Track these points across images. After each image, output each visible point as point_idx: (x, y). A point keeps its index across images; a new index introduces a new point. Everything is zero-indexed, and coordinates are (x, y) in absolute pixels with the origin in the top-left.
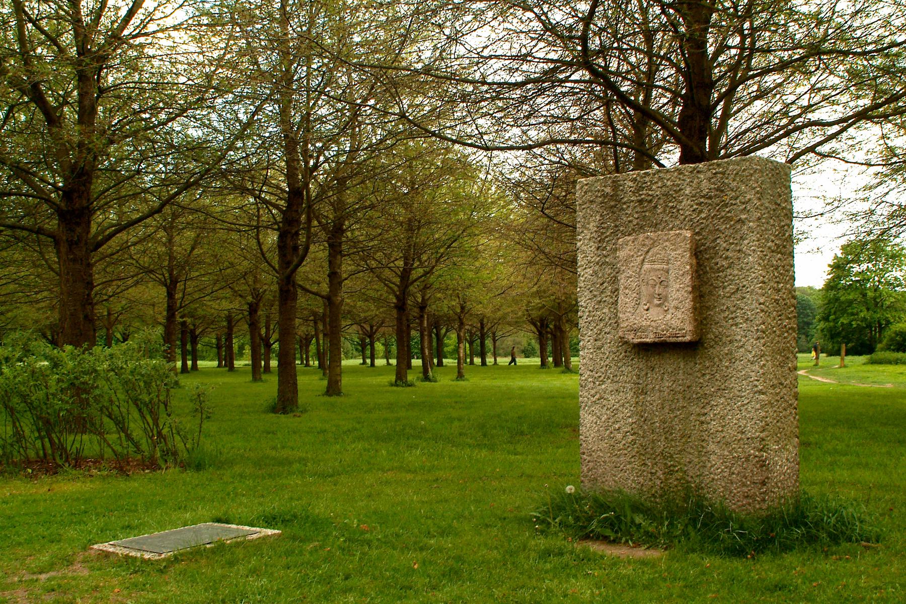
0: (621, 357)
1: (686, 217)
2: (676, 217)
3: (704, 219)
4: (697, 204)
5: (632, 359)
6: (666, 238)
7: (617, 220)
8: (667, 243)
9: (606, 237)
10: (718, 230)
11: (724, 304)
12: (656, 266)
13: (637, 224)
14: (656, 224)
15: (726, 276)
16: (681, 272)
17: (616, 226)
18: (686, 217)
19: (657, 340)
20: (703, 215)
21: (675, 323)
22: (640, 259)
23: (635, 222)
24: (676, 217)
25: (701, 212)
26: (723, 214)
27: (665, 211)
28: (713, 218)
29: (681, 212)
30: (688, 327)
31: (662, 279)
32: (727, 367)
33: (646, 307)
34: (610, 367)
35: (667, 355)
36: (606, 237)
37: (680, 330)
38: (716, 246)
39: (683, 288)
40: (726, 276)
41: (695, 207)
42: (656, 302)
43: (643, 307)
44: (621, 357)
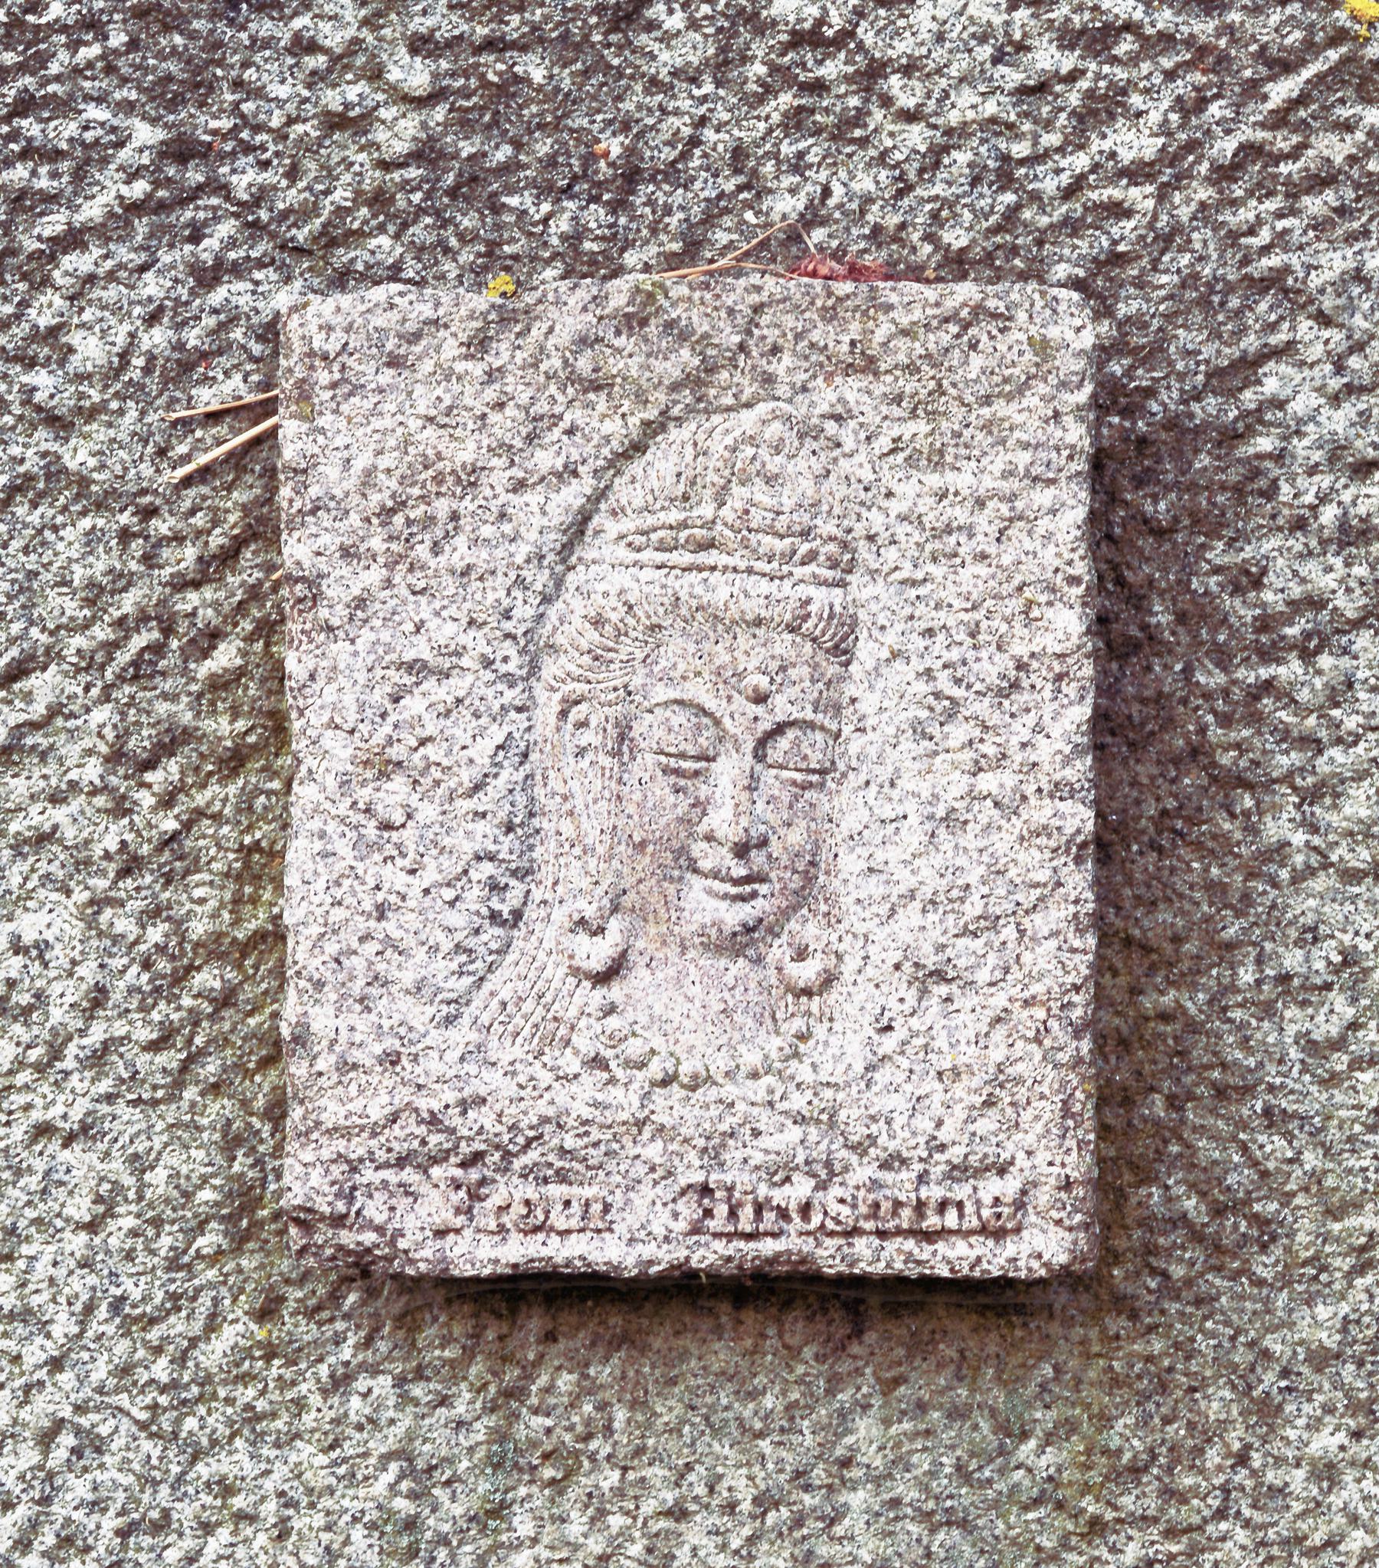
0: (214, 1353)
1: (956, 135)
2: (846, 130)
3: (1137, 173)
4: (1068, 37)
5: (340, 1383)
6: (839, 339)
7: (199, 86)
8: (852, 389)
9: (73, 239)
10: (1274, 281)
11: (1311, 936)
12: (720, 591)
13: (427, 153)
14: (631, 175)
15: (1341, 692)
16: (991, 668)
17: (181, 150)
18: (956, 135)
19: (707, 1255)
20: (1132, 142)
21: (916, 1110)
22: (543, 513)
23: (400, 131)
24: (846, 130)
25: (1104, 108)
26: (1334, 148)
27: (724, 65)
28: (1224, 174)
29: (904, 92)
30: (1046, 1153)
31: (782, 707)
32: (1327, 1473)
33: (597, 953)
34: (92, 1444)
35: (722, 1354)
36: (73, 239)
37: (959, 1172)
38: (1254, 420)
39: (1008, 807)
40: (1341, 692)
41: (1047, 57)
42: (706, 906)
43: (550, 947)
44: (214, 1353)
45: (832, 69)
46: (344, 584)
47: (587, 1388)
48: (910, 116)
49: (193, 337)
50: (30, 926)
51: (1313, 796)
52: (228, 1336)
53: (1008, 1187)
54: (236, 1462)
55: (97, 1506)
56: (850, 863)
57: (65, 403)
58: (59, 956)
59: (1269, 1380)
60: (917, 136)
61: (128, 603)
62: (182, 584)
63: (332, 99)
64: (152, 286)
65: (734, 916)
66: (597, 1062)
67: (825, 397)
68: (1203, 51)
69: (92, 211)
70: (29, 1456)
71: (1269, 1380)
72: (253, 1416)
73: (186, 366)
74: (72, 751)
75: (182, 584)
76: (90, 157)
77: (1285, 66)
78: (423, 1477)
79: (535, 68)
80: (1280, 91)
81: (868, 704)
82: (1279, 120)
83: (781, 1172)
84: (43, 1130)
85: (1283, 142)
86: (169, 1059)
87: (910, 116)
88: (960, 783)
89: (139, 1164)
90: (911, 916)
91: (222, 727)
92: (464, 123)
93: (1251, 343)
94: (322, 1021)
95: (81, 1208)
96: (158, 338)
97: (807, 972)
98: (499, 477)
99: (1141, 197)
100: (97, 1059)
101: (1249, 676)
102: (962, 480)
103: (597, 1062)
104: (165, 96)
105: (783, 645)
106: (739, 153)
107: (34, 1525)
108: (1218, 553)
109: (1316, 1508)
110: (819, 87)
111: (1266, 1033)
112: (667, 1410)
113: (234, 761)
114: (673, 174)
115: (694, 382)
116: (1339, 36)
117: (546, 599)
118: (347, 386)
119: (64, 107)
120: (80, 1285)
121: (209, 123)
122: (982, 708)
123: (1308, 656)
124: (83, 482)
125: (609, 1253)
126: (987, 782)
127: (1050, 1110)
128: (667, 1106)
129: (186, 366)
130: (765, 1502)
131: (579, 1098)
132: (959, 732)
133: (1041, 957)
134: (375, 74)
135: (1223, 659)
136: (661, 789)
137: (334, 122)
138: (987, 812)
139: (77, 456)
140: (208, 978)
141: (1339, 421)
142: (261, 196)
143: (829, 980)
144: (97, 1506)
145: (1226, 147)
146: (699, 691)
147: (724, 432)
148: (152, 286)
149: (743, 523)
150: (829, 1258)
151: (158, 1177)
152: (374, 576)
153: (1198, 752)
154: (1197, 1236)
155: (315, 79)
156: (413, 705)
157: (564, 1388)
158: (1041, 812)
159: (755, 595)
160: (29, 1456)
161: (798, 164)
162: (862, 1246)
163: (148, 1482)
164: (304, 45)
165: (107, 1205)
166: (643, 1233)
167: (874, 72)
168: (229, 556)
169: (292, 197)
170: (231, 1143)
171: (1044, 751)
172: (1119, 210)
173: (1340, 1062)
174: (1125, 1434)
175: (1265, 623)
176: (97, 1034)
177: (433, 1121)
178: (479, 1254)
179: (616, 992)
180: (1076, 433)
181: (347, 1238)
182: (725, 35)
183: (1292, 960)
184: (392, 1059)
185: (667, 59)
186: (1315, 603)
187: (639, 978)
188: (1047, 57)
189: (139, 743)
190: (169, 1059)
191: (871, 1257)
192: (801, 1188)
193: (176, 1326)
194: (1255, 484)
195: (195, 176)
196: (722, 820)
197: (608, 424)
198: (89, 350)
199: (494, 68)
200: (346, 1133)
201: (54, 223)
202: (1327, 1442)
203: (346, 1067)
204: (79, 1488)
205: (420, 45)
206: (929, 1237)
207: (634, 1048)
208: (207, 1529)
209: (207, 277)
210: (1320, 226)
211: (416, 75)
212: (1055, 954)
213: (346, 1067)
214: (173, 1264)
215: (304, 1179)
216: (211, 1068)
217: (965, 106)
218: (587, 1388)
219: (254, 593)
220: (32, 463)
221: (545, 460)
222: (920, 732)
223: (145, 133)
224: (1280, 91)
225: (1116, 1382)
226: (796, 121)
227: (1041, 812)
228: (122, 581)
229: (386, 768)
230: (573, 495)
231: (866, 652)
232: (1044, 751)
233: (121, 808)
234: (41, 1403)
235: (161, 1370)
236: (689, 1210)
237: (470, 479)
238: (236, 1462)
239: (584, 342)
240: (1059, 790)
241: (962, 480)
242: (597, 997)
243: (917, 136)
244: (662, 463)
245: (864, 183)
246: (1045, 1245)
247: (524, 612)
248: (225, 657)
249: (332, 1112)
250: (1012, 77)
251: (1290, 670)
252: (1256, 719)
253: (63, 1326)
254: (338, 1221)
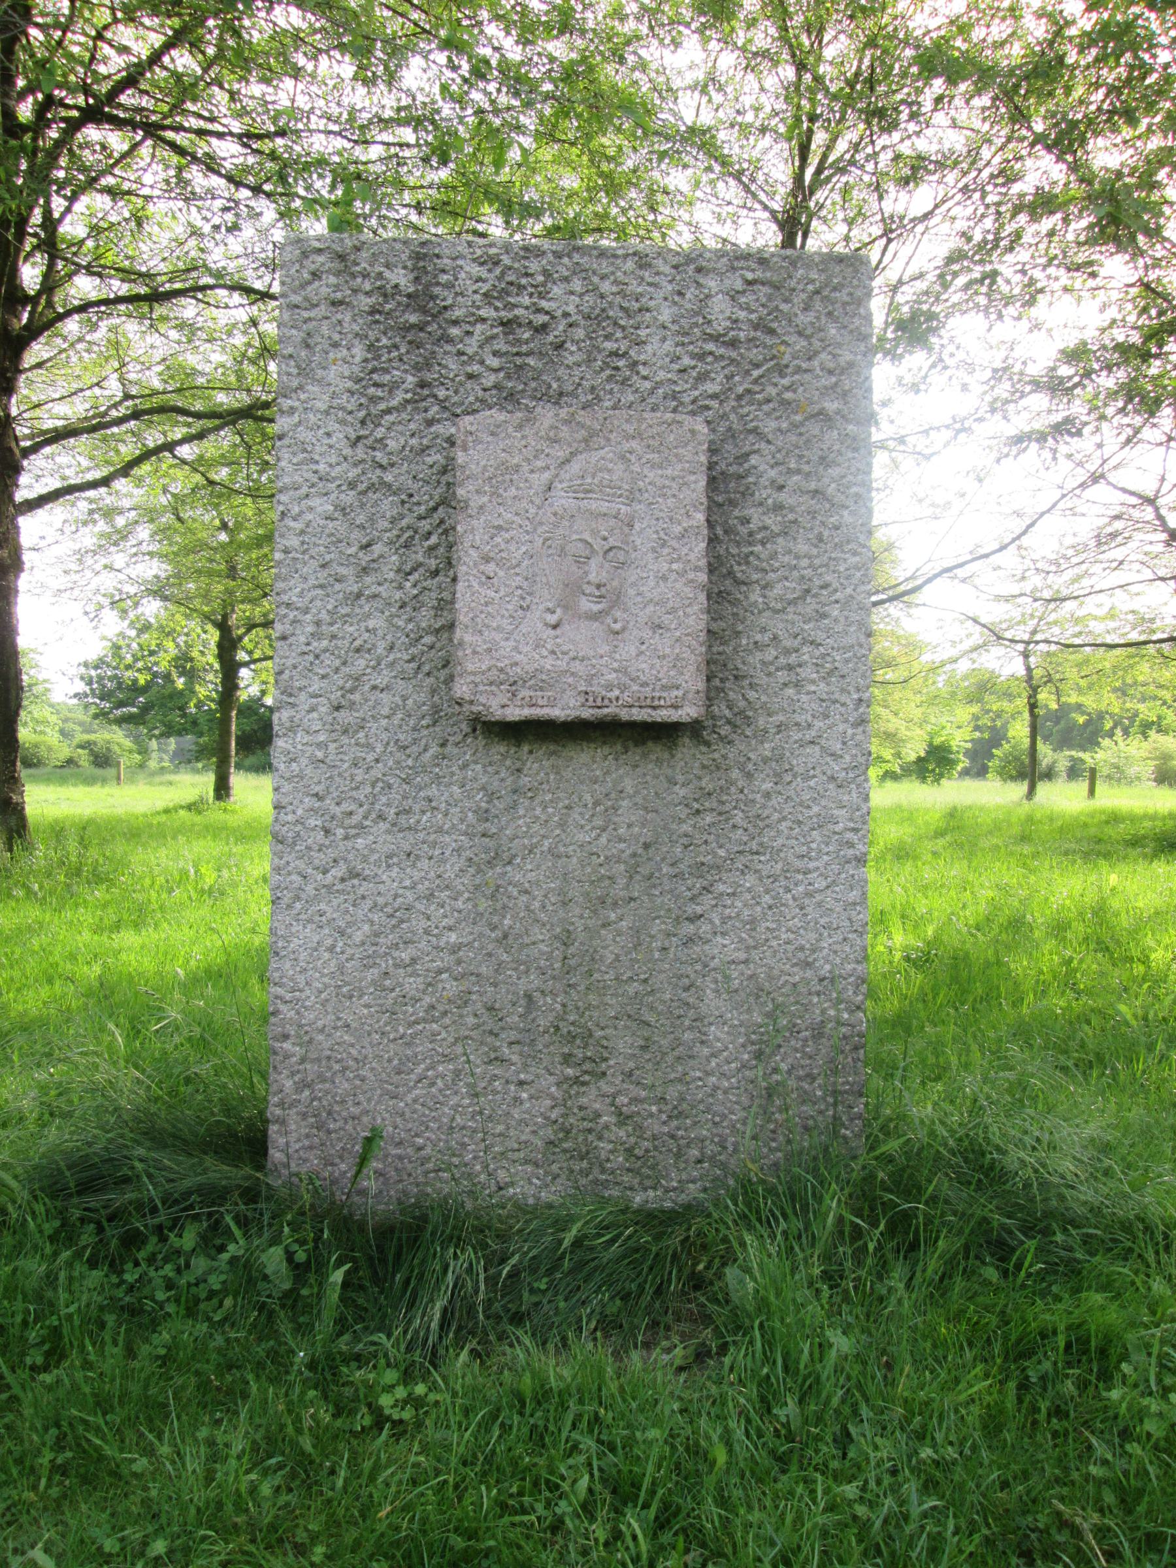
1: (658, 385)
3: (714, 396)
4: (693, 356)
5: (465, 766)
7: (428, 366)
8: (634, 444)
9: (388, 411)
10: (754, 431)
11: (764, 630)
12: (594, 505)
13: (497, 386)
16: (677, 529)
17: (422, 384)
18: (658, 385)
20: (711, 388)
23: (490, 380)
25: (703, 377)
27: (590, 361)
28: (739, 398)
29: (644, 371)
30: (692, 681)
31: (612, 542)
32: (767, 795)
33: (552, 619)
36: (388, 411)
37: (664, 688)
38: (748, 473)
41: (687, 361)
45: (621, 363)
46: (476, 501)
47: (542, 768)
48: (645, 378)
49: (425, 442)
50: (371, 624)
51: (764, 587)
52: (431, 752)
53: (680, 693)
54: (433, 791)
55: (388, 805)
56: (632, 592)
57: (384, 462)
58: (380, 633)
59: (750, 766)
60: (647, 385)
61: (404, 523)
62: (420, 518)
63: (469, 369)
64: (412, 426)
65: (596, 608)
66: (553, 652)
67: (627, 446)
68: (733, 360)
69: (394, 403)
70: (368, 789)
71: (750, 766)
72: (438, 777)
73: (424, 450)
74: (385, 569)
75: (420, 518)
76: (393, 387)
77: (757, 366)
78: (491, 796)
79: (531, 361)
80: (756, 373)
81: (638, 542)
82: (756, 382)
83: (609, 687)
84: (374, 688)
85: (757, 388)
86: (413, 665)
87: (645, 378)
88: (666, 566)
89: (405, 699)
90: (651, 608)
91: (433, 563)
92: (508, 377)
93: (747, 449)
94: (468, 638)
95: (386, 711)
96: (414, 442)
97: (617, 626)
98: (526, 468)
99: (714, 404)
100: (392, 664)
101: (745, 550)
102: (669, 472)
103: (553, 652)
104: (417, 368)
105: (612, 522)
106: (593, 388)
107: (369, 812)
108: (736, 513)
109: (764, 807)
110: (617, 369)
111: (750, 659)
112: (567, 773)
113: (435, 573)
114: (573, 394)
115: (586, 441)
116: (773, 357)
117: (615, 324)
118: (477, 441)
119: (386, 371)
120: (385, 736)
121: (429, 376)
122: (674, 543)
123: (763, 544)
124: (390, 486)
125: (558, 713)
126: (675, 566)
127: (692, 668)
128: (577, 666)
129: (424, 450)
130: (597, 803)
131: (548, 663)
132: (666, 551)
133: (691, 621)
134: (482, 362)
135: (738, 544)
136: (574, 568)
137: (470, 376)
138: (674, 576)
139: (389, 478)
140: (428, 640)
141: (773, 473)
142: (447, 398)
143: (624, 629)
144: (388, 805)
145: (740, 390)
146: (587, 536)
147: (595, 456)
148: (412, 426)
149: (601, 484)
150: (625, 715)
151: (410, 702)
152: (485, 499)
153: (730, 573)
154: (729, 722)
155: (464, 363)
156: (498, 540)
157: (537, 764)
158: (691, 575)
159: (604, 507)
160: (368, 789)
161: (611, 392)
162: (634, 711)
163: (405, 798)
164: (460, 353)
165: (394, 710)
166: (565, 708)
167: (635, 363)
168: (435, 509)
169: (456, 399)
170: (433, 692)
171: (692, 557)
172: (707, 408)
173: (772, 669)
174: (707, 783)
175: (751, 534)
176: (391, 657)
177: (501, 670)
178: (515, 713)
179: (558, 632)
180: (703, 459)
181: (475, 709)
182: (589, 353)
183: (758, 637)
184: (489, 650)
185: (570, 360)
186: (766, 528)
187: (566, 627)
188: (687, 361)
189: (408, 568)
190: (413, 665)
191: (638, 715)
192: (617, 692)
193: (415, 749)
194: (746, 493)
195: (426, 392)
196: (592, 577)
197: (560, 453)
198: (392, 444)
199: (519, 360)
200: (474, 673)
201: (382, 406)
202: (768, 786)
203: (475, 652)
204: (384, 799)
205: (495, 354)
206: (654, 708)
207: (565, 648)
208: (423, 812)
209: (430, 423)
210: (768, 414)
211: (495, 362)
212: (695, 619)
213: (475, 652)
214: (414, 729)
215: (461, 689)
216: (426, 668)
217: (662, 375)
218: (542, 768)
219: (442, 522)
220: (375, 479)
221: (539, 464)
222: (654, 550)
223: (410, 379)
224: (756, 373)
225: (704, 767)
226: (610, 378)
227: (691, 575)
228: (402, 516)
229: (487, 559)
230: (547, 475)
231: (637, 526)
232: (692, 557)
233: (400, 587)
234: (373, 772)
235: (410, 762)
236: (582, 699)
237: (517, 468)
238: (433, 791)
239: (552, 427)
240: (697, 569)
241: (669, 472)
242: (552, 633)
243: (647, 385)
244: (575, 467)
245: (631, 398)
246: (689, 712)
247: (532, 511)
248: (434, 539)
249: (470, 667)
250: (676, 367)
251: (758, 548)
252: (748, 563)
253: (379, 749)
254: (471, 702)
